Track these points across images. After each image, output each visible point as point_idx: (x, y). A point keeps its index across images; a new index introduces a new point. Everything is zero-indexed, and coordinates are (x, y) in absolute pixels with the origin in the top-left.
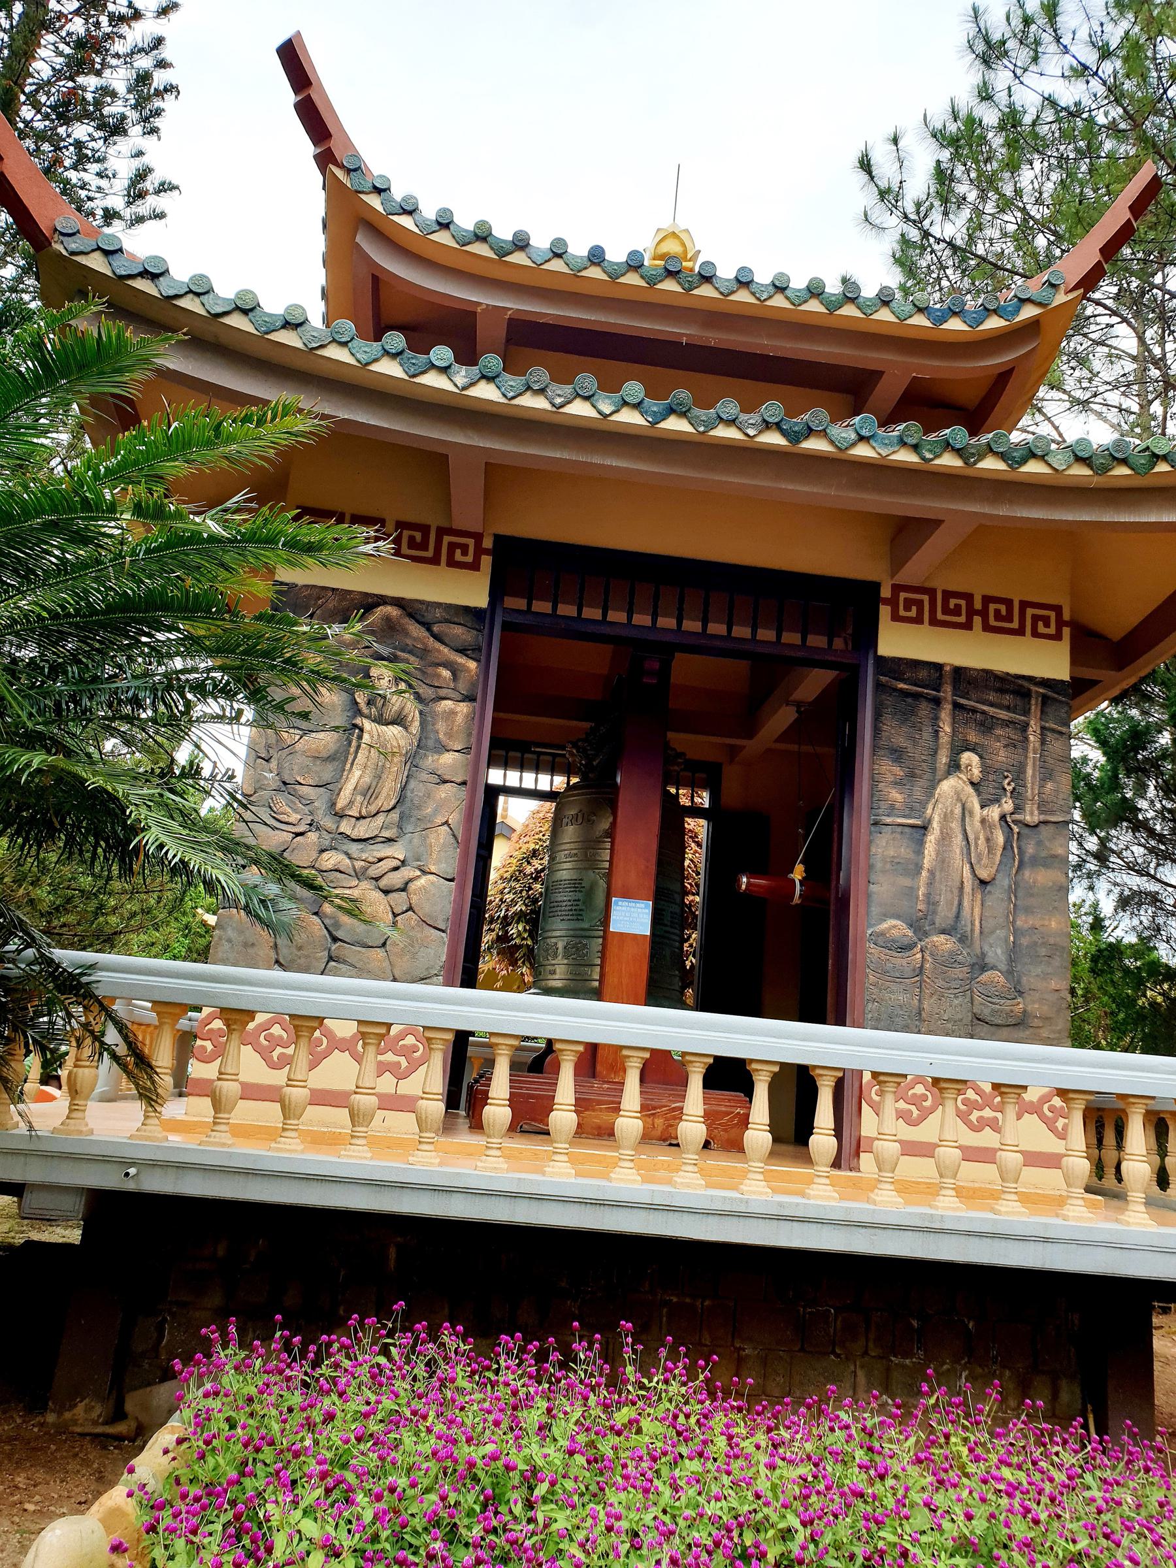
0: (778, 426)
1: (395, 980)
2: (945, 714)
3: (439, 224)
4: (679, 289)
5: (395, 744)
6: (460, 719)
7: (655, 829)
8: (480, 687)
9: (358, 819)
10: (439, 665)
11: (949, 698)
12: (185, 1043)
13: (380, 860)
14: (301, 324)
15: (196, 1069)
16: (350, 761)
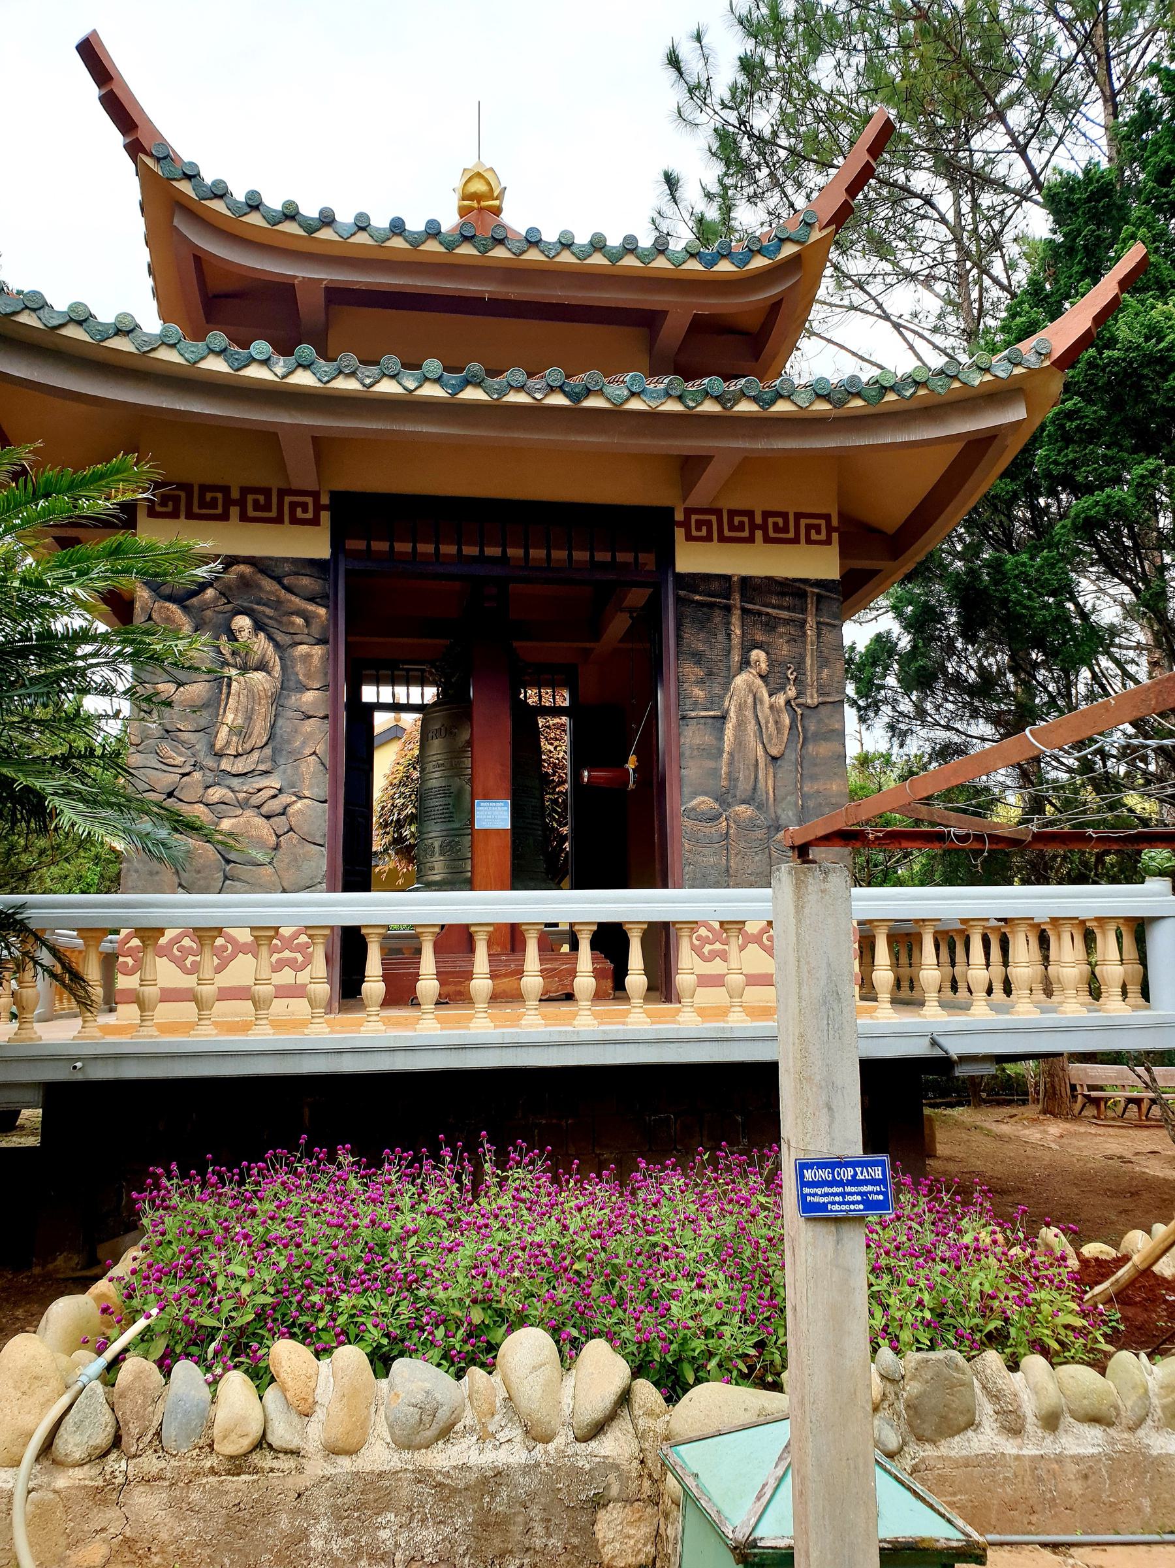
0: (561, 389)
1: (284, 891)
2: (735, 619)
3: (250, 206)
4: (476, 253)
6: (316, 661)
8: (331, 630)
9: (235, 756)
10: (292, 614)
12: (109, 962)
13: (259, 790)
14: (131, 331)
15: (124, 982)
16: (222, 707)
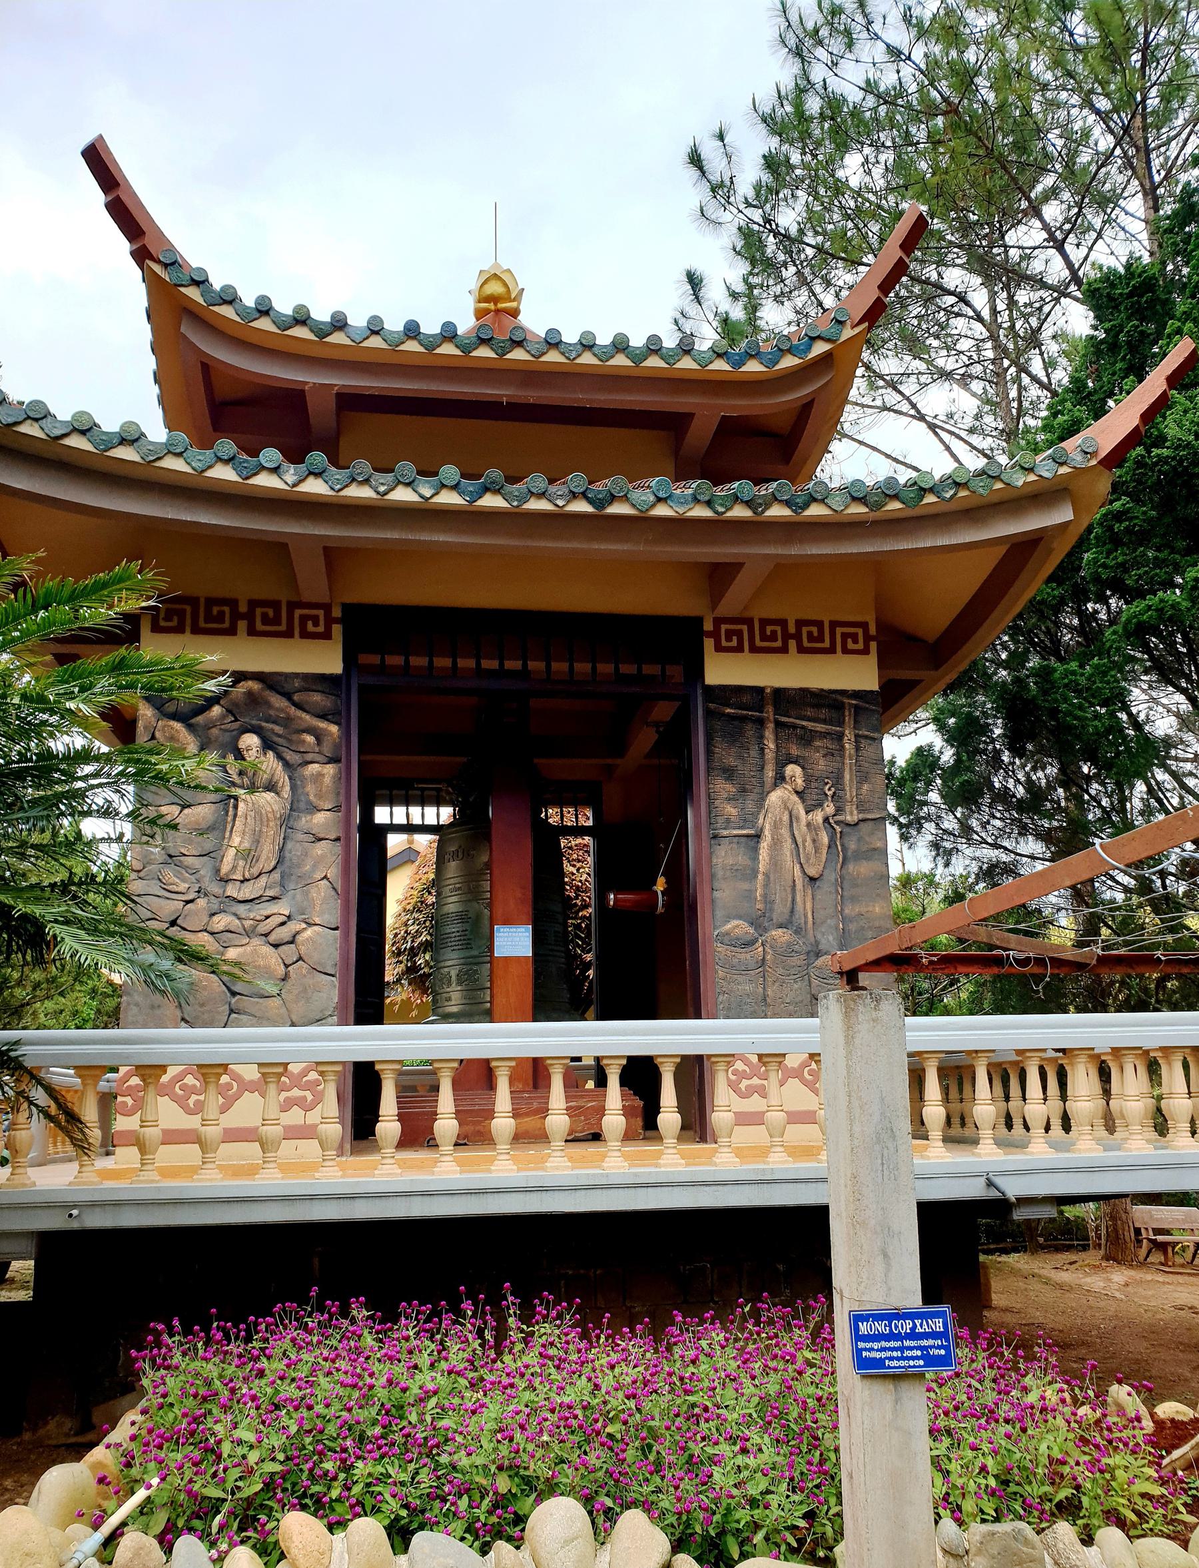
0: (584, 495)
1: (293, 1025)
2: (769, 734)
3: (259, 311)
5: (269, 809)
6: (327, 780)
7: (529, 859)
9: (242, 882)
11: (772, 718)
12: (107, 1101)
13: (267, 917)
14: (137, 440)
15: (122, 1123)
16: (229, 829)
